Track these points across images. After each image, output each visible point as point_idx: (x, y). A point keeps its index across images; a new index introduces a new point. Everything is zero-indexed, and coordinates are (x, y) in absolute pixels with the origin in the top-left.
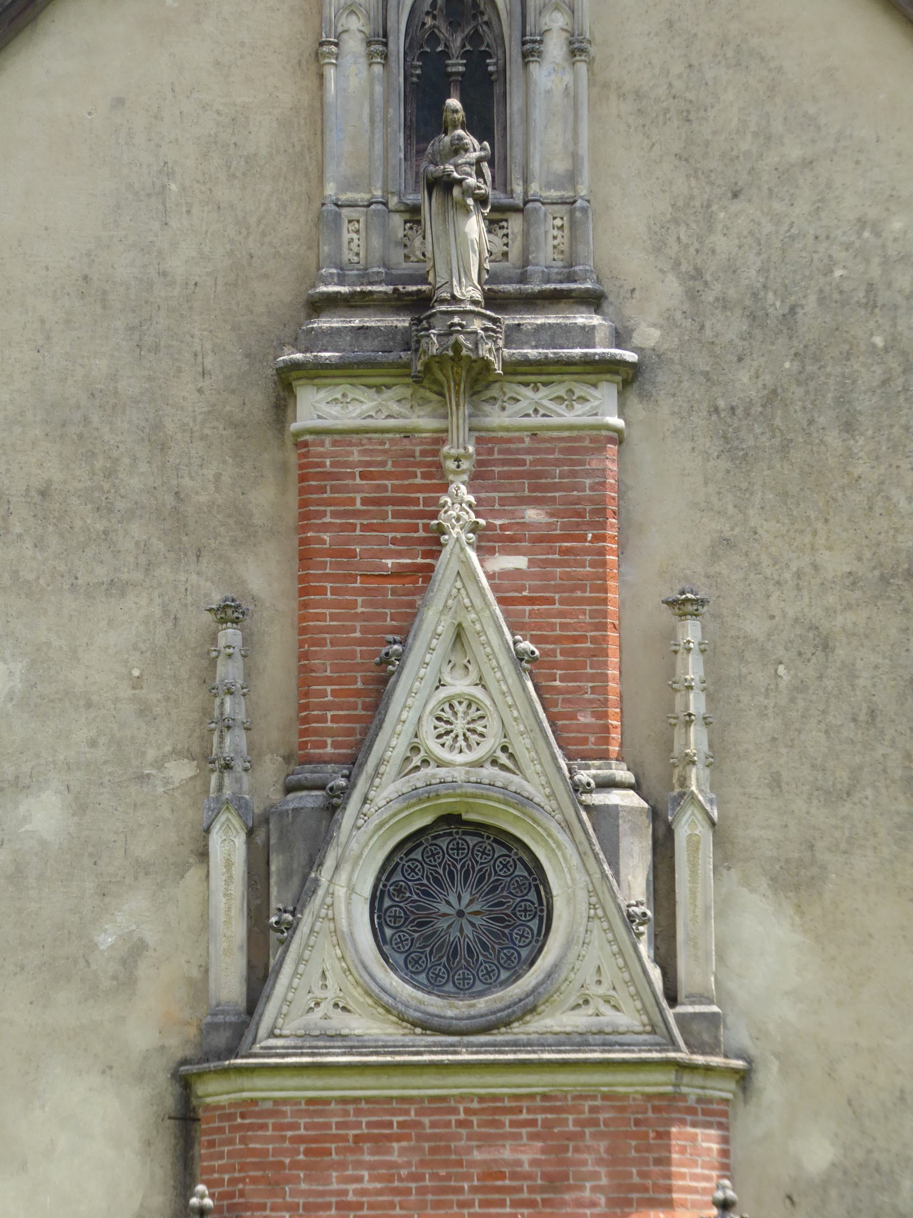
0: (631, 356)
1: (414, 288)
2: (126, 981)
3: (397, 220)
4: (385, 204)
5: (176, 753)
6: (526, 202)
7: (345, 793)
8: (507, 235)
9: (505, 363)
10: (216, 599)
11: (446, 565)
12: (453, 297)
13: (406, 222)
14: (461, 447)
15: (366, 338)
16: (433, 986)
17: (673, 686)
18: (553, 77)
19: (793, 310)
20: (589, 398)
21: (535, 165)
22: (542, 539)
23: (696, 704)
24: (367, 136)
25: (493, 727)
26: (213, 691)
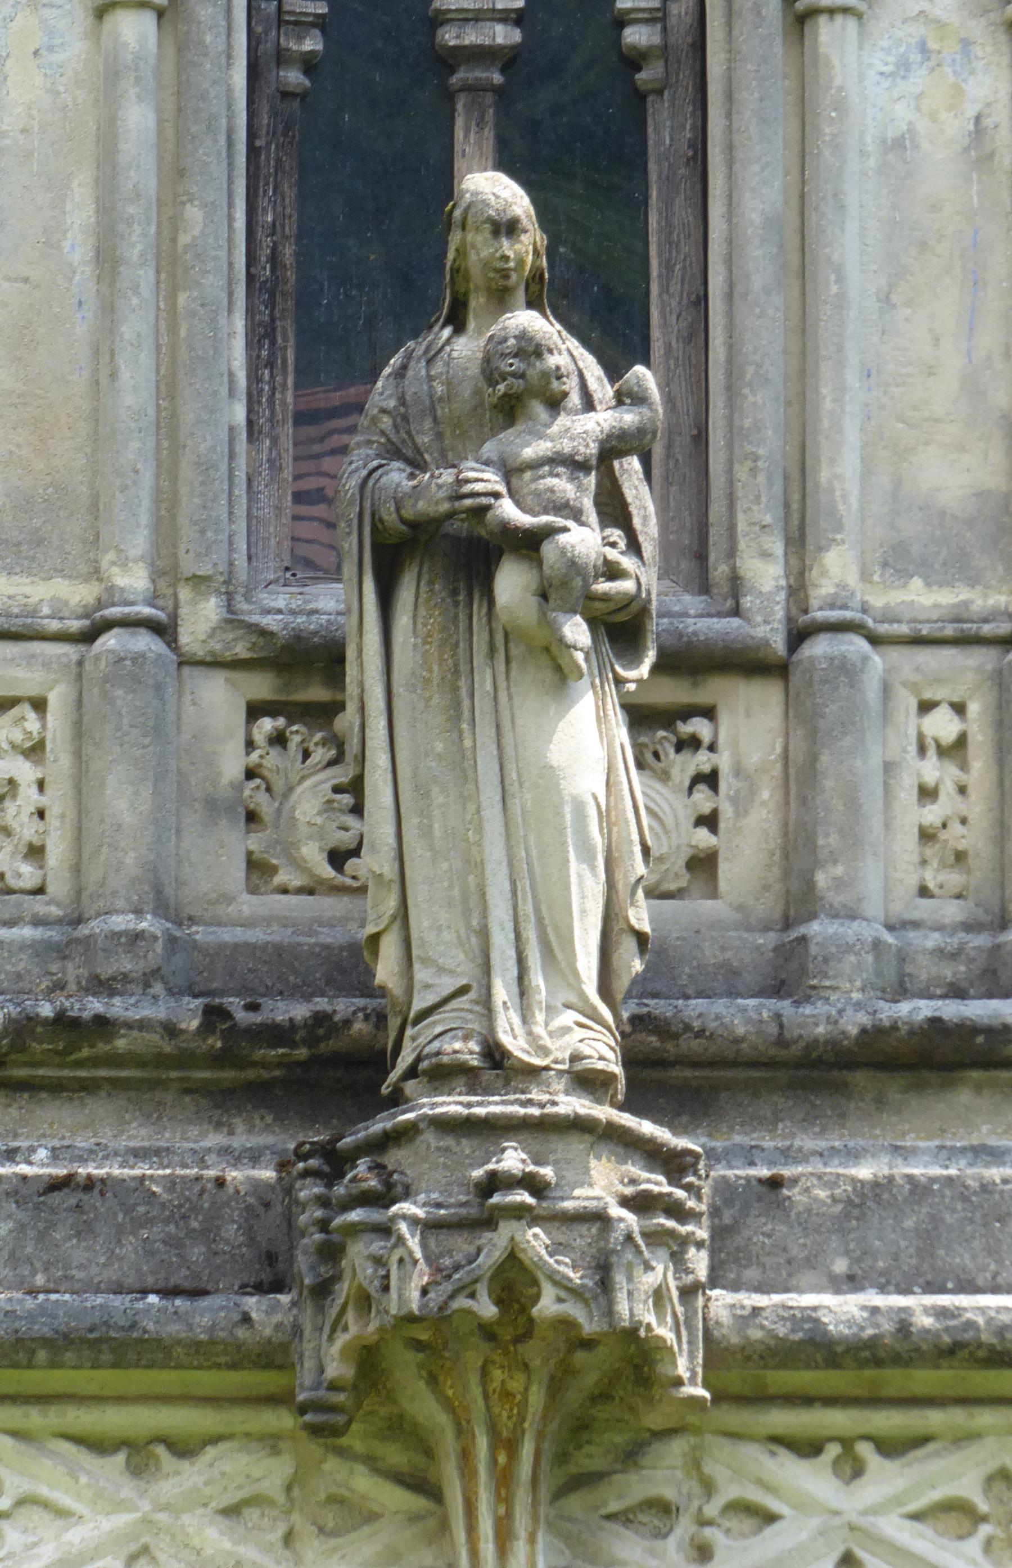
1: (300, 1011)
3: (218, 703)
4: (164, 630)
6: (799, 635)
8: (710, 779)
9: (716, 1354)
12: (495, 1055)
13: (255, 711)
15: (84, 1231)
18: (919, 80)
20: (774, 1505)
21: (843, 472)
24: (82, 326)
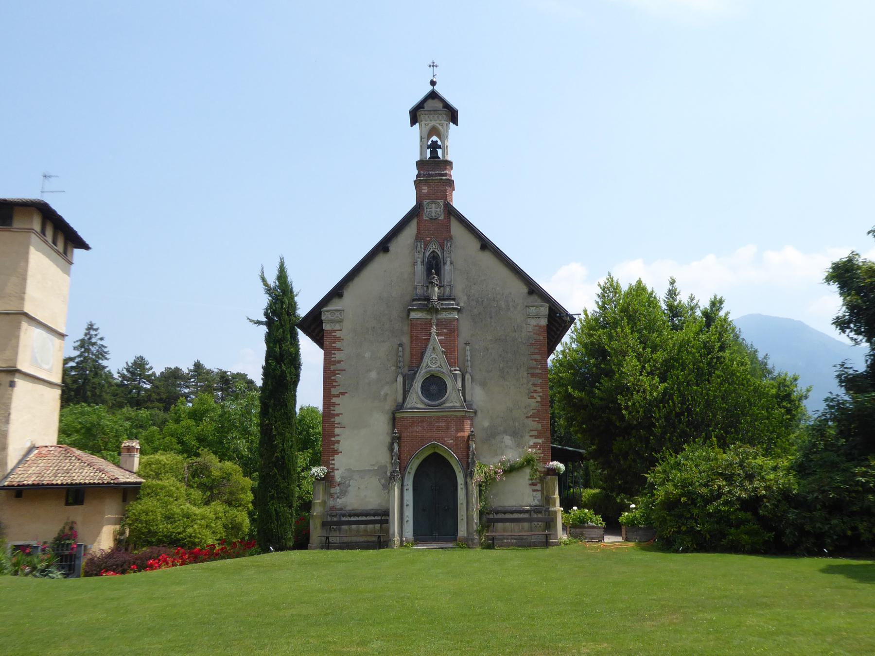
14: (434, 321)
17: (465, 355)
22: (446, 334)
23: (469, 358)
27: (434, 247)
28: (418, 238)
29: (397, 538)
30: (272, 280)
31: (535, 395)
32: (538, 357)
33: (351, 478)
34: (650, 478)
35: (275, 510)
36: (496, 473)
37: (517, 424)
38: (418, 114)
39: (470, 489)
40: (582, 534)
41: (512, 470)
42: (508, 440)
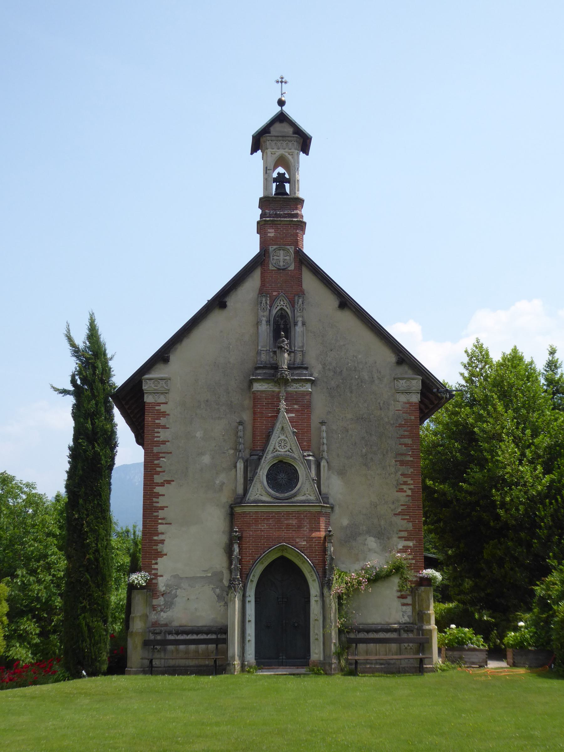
0: (313, 379)
2: (221, 489)
3: (271, 353)
5: (231, 448)
7: (262, 456)
9: (291, 379)
10: (238, 421)
11: (280, 415)
14: (283, 394)
16: (277, 491)
17: (320, 438)
19: (341, 371)
21: (296, 344)
22: (297, 411)
23: (325, 441)
25: (288, 445)
26: (237, 437)
27: (282, 304)
28: (262, 292)
29: (237, 662)
30: (81, 340)
31: (405, 487)
32: (409, 441)
33: (178, 587)
34: (539, 590)
35: (87, 625)
36: (360, 583)
37: (383, 523)
38: (262, 140)
39: (327, 601)
40: (461, 658)
41: (377, 578)
42: (372, 542)
